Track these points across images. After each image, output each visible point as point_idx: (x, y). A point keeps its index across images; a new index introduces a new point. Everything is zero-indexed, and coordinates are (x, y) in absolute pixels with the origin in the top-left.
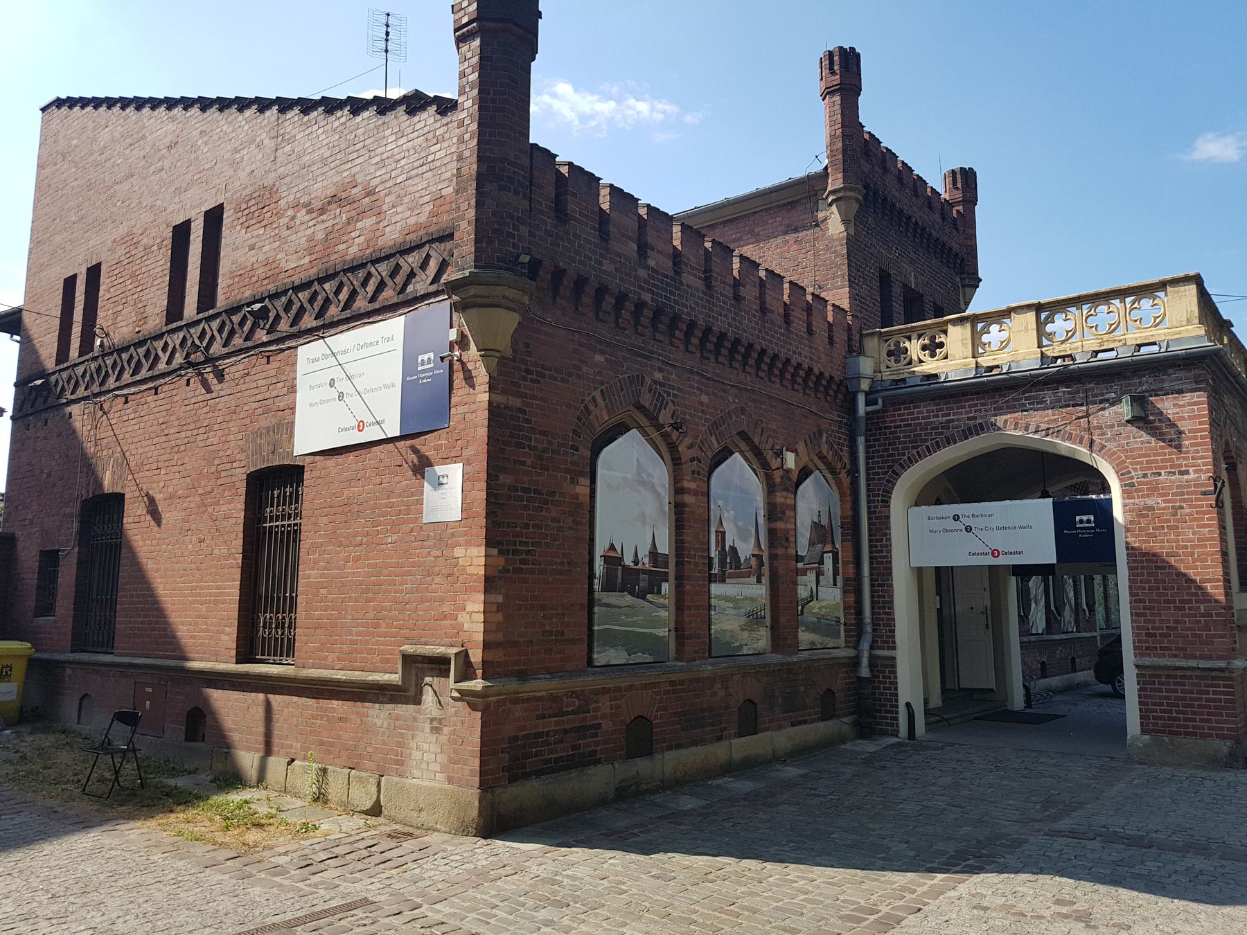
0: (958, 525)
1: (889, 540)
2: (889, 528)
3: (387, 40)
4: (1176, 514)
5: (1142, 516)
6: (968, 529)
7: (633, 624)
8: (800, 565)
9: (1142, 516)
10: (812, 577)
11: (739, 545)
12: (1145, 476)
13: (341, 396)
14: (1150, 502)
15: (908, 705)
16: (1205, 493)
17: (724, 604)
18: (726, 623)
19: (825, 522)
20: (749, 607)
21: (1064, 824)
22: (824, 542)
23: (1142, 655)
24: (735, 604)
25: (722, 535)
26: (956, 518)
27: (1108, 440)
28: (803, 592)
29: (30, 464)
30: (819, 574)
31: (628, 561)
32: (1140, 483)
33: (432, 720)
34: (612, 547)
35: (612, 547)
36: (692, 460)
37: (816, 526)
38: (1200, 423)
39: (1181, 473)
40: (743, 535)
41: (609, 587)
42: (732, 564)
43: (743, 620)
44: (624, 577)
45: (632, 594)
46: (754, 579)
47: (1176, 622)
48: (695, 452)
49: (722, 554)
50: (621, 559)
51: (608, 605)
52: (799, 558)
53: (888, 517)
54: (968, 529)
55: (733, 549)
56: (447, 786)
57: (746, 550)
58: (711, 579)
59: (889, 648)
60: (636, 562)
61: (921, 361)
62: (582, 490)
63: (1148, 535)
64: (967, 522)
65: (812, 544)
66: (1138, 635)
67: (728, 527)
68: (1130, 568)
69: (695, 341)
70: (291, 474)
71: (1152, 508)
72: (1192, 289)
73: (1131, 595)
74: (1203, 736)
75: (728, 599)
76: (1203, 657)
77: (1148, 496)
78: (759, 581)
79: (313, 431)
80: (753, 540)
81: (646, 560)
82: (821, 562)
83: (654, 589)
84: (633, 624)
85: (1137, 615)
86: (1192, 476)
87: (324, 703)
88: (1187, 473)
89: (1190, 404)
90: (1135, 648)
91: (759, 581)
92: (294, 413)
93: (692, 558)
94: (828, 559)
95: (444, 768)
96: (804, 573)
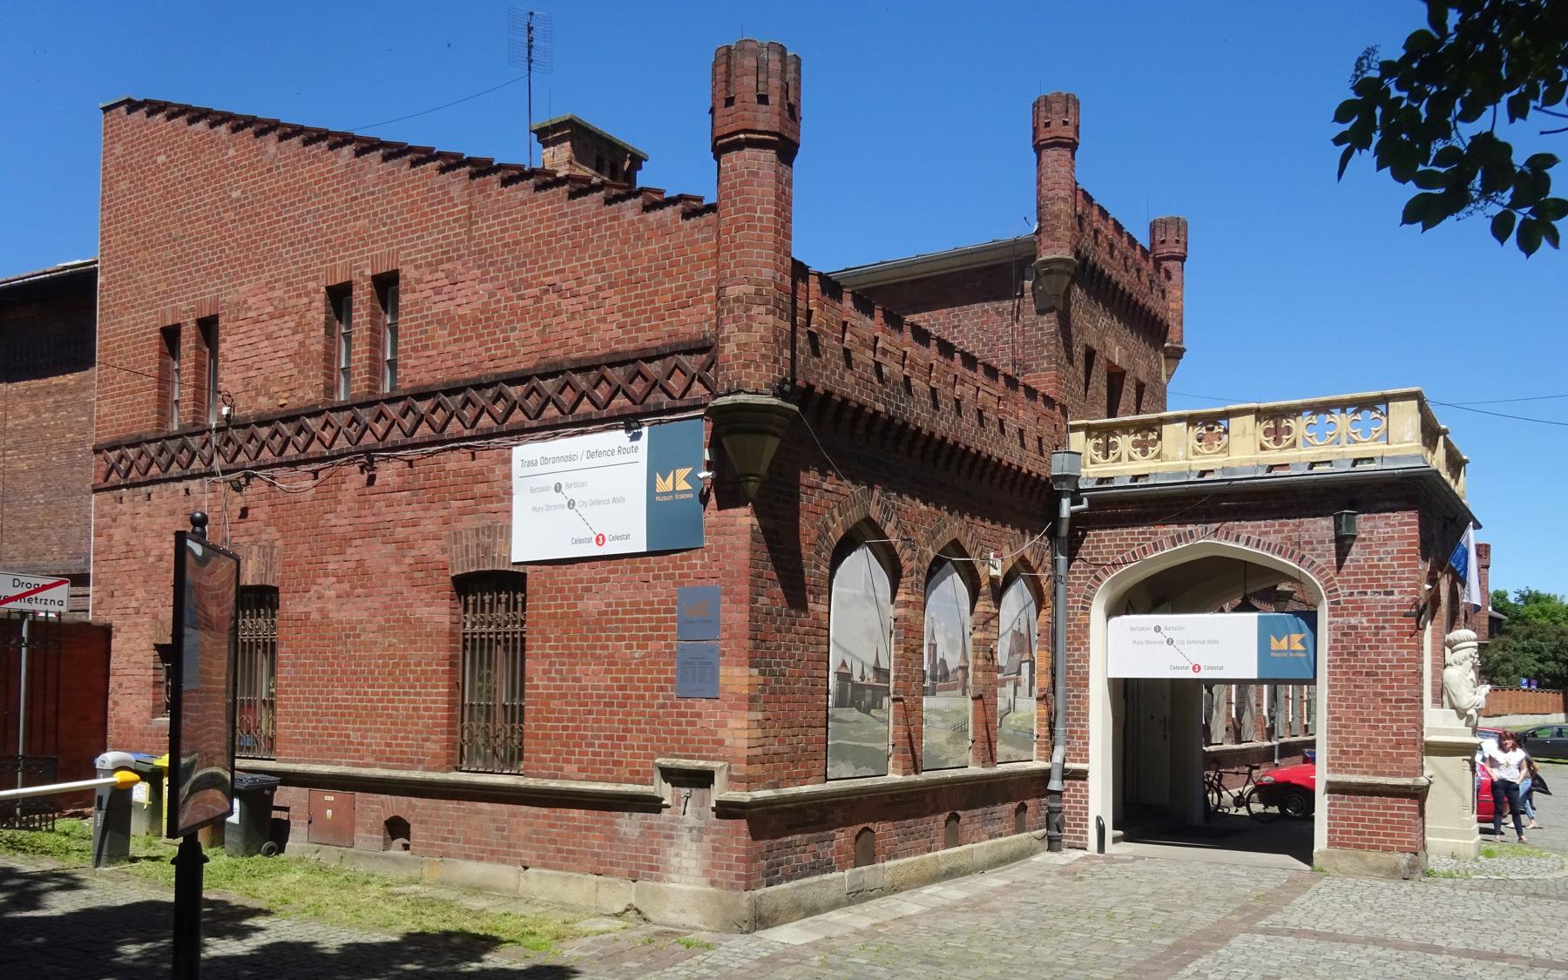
0: (1159, 636)
1: (1088, 649)
2: (1087, 636)
3: (530, 47)
4: (1377, 634)
5: (1344, 634)
6: (1170, 642)
7: (859, 739)
8: (1000, 676)
9: (1344, 634)
10: (1010, 688)
11: (948, 657)
12: (1351, 594)
13: (571, 504)
14: (1353, 621)
15: (1099, 819)
16: (1406, 615)
17: (934, 717)
18: (934, 737)
19: (1024, 631)
20: (955, 720)
21: (1262, 923)
22: (1021, 651)
23: (1335, 771)
24: (944, 712)
25: (933, 646)
26: (1158, 629)
27: (1318, 556)
28: (1002, 704)
29: (128, 544)
30: (1017, 684)
31: (856, 678)
32: (1346, 602)
33: (691, 829)
34: (844, 664)
35: (844, 664)
36: (912, 571)
37: (1017, 635)
38: (1410, 544)
39: (1387, 593)
40: (951, 644)
41: (840, 703)
42: (942, 675)
43: (950, 733)
44: (856, 695)
45: (859, 709)
46: (959, 692)
47: (1370, 740)
48: (914, 563)
49: (934, 667)
50: (850, 675)
51: (840, 721)
52: (1000, 669)
53: (1087, 625)
54: (1170, 642)
55: (943, 662)
56: (711, 889)
57: (953, 661)
58: (925, 692)
59: (1082, 761)
60: (863, 678)
61: (1131, 459)
62: (821, 608)
63: (1349, 654)
64: (1169, 634)
65: (1011, 653)
66: (1332, 752)
67: (940, 640)
68: (1330, 686)
69: (916, 452)
70: (511, 582)
71: (1354, 627)
72: (1413, 404)
73: (1330, 713)
74: (1386, 850)
75: (937, 712)
76: (1392, 774)
77: (1354, 615)
78: (964, 694)
79: (533, 536)
80: (960, 652)
81: (871, 676)
82: (1019, 672)
83: (876, 704)
84: (859, 739)
85: (1334, 732)
86: (1396, 597)
87: (559, 812)
88: (1392, 593)
89: (1401, 524)
90: (1329, 765)
91: (964, 694)
92: (510, 517)
93: (911, 676)
94: (1025, 668)
95: (706, 873)
96: (1003, 683)
